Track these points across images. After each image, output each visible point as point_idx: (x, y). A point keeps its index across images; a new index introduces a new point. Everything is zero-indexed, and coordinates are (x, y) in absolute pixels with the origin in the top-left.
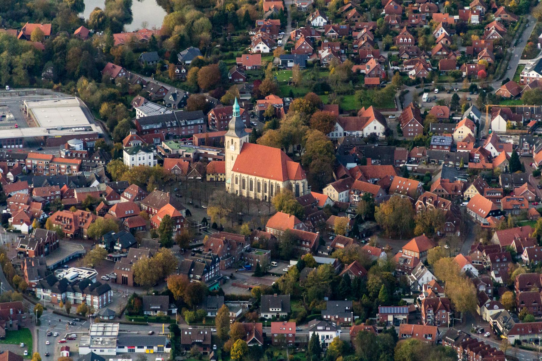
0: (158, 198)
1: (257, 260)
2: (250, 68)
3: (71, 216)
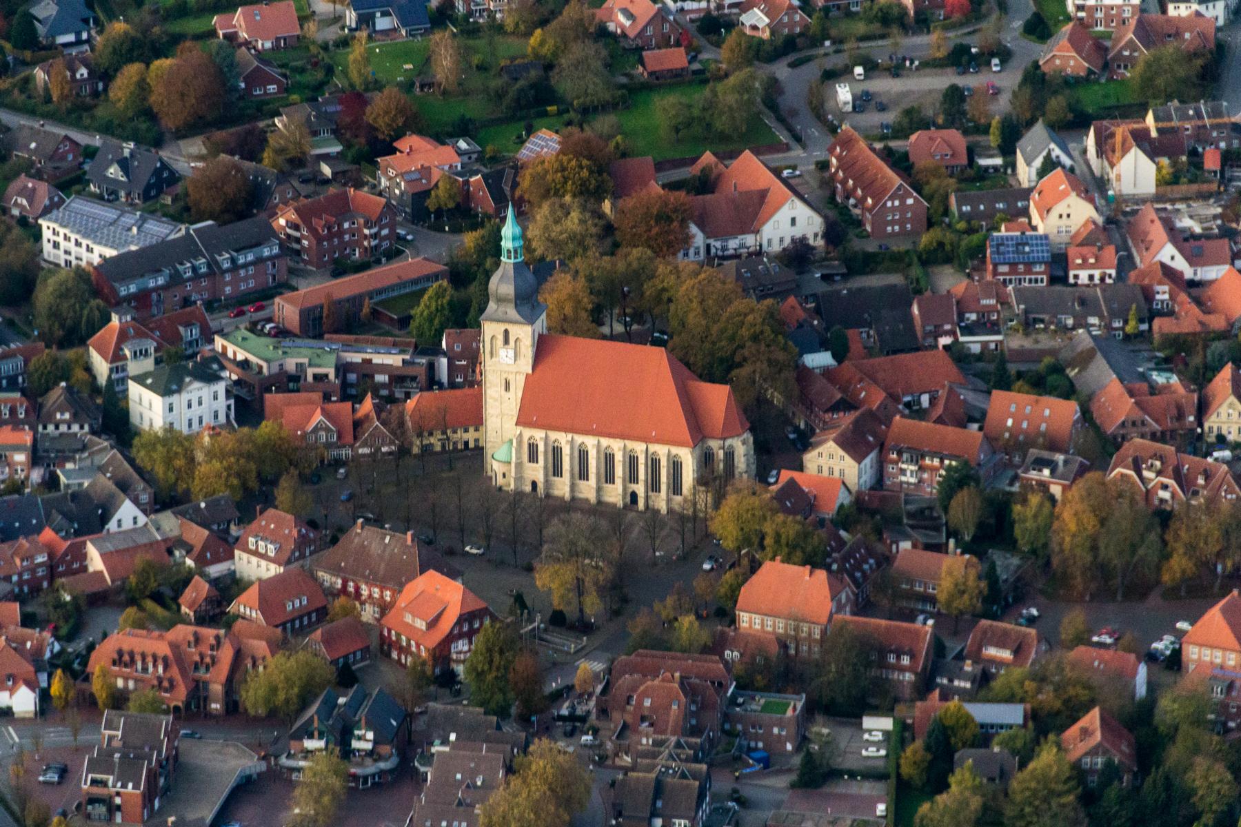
0: (375, 548)
1: (776, 730)
2: (268, 45)
3: (163, 649)
